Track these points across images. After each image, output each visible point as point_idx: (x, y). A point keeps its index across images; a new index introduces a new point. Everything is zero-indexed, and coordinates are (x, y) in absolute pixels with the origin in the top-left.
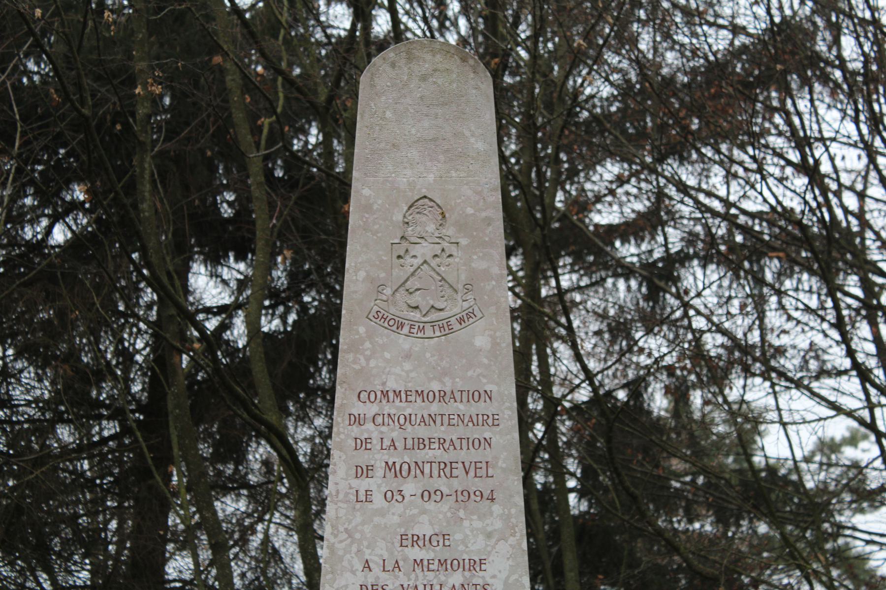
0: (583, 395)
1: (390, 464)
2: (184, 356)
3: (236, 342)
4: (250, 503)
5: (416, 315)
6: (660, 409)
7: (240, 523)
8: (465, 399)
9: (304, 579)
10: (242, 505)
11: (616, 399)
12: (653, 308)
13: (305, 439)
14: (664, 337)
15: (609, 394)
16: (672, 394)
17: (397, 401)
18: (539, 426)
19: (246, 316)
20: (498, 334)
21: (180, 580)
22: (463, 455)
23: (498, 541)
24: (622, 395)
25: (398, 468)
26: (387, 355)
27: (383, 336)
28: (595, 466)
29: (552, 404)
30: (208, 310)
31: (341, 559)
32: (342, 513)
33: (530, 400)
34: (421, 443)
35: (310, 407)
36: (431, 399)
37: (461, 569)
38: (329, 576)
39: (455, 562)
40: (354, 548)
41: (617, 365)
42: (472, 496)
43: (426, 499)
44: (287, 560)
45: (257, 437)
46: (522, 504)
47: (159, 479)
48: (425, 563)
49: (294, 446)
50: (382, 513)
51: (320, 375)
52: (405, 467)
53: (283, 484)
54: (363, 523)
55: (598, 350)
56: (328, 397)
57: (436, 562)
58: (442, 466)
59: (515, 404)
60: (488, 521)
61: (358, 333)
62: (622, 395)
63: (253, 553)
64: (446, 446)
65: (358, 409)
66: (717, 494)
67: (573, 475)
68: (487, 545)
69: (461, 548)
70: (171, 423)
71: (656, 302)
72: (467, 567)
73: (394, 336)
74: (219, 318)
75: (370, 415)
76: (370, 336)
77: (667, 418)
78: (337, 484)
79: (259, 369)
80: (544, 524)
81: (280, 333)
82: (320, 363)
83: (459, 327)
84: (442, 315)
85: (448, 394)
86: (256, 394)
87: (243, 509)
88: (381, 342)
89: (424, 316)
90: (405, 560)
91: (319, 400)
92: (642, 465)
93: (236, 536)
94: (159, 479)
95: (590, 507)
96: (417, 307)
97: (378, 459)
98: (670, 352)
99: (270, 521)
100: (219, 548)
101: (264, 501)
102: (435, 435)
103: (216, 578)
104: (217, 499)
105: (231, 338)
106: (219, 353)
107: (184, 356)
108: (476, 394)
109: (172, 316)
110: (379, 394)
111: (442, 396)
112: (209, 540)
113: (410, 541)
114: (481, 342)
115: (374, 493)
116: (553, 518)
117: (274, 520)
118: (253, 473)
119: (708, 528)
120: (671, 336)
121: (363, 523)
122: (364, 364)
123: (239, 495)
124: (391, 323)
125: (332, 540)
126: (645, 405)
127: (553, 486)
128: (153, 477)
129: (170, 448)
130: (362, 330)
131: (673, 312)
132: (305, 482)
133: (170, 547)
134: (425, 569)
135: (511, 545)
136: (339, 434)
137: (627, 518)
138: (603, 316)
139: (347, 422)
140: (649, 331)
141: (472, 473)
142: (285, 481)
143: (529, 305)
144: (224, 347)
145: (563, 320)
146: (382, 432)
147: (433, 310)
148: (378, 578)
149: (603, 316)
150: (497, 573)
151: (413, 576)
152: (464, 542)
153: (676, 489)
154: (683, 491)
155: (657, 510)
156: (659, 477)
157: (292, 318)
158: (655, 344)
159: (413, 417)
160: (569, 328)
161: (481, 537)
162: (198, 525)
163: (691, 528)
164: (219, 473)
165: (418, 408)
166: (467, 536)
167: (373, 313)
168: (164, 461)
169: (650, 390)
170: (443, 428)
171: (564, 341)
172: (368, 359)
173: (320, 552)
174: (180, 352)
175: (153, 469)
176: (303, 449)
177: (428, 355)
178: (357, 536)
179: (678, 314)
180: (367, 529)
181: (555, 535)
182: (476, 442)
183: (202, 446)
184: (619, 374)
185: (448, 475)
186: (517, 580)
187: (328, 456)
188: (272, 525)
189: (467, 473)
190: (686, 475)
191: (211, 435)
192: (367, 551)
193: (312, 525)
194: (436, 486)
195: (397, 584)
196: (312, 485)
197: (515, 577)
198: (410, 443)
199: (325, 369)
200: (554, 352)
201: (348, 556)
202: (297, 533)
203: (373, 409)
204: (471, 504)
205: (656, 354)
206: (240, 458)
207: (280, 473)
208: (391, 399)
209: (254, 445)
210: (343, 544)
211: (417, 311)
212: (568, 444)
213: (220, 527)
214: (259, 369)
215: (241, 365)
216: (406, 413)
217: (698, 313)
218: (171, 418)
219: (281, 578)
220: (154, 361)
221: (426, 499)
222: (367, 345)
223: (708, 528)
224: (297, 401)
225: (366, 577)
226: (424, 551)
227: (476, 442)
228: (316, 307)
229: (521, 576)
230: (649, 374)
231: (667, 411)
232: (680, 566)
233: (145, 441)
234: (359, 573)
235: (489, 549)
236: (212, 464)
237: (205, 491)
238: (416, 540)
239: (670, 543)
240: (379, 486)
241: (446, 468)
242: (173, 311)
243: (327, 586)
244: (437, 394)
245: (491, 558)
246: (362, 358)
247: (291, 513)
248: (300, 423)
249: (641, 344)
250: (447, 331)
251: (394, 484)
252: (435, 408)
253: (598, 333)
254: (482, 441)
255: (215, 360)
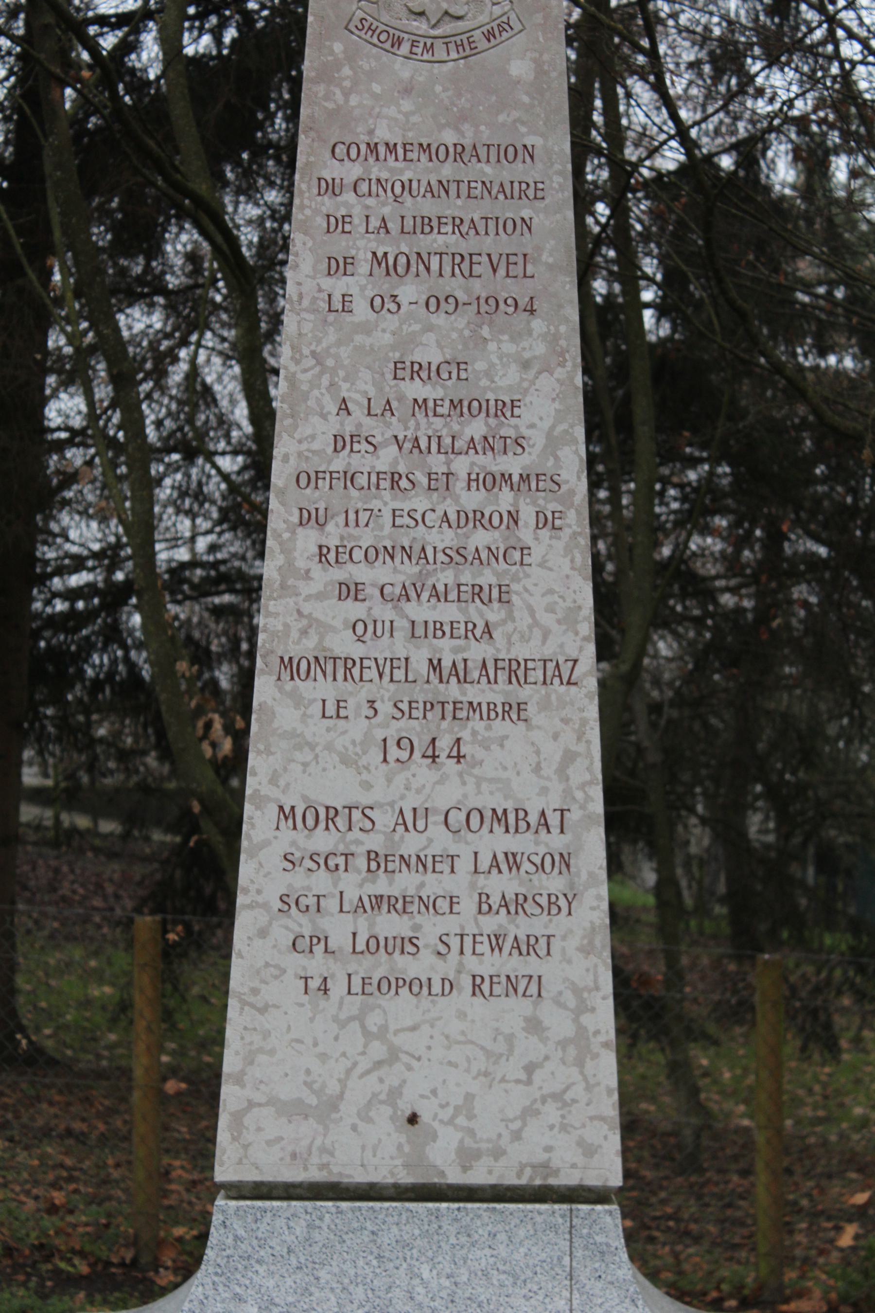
0: (671, 158)
1: (380, 255)
2: (69, 91)
3: (145, 70)
4: (167, 318)
5: (420, 26)
6: (783, 185)
7: (153, 346)
8: (493, 158)
9: (249, 429)
10: (157, 320)
11: (718, 168)
12: (780, 26)
13: (250, 222)
14: (796, 70)
15: (709, 159)
16: (804, 160)
17: (391, 159)
18: (601, 208)
19: (160, 31)
20: (546, 57)
21: (67, 429)
22: (488, 243)
23: (540, 373)
24: (726, 162)
25: (433, 151)
26: (376, 88)
27: (371, 58)
28: (684, 268)
29: (622, 171)
30: (102, 20)
31: (305, 397)
32: (307, 328)
33: (588, 169)
34: (427, 225)
35: (258, 175)
36: (442, 156)
37: (483, 414)
38: (288, 422)
39: (475, 404)
40: (325, 381)
41: (721, 115)
42: (502, 305)
43: (433, 308)
44: (224, 403)
45: (178, 217)
46: (577, 318)
47: (32, 276)
48: (431, 404)
49: (235, 232)
50: (366, 329)
51: (273, 124)
52: (402, 260)
53: (218, 290)
54: (339, 343)
55: (694, 91)
56: (284, 158)
57: (447, 403)
58: (458, 259)
59: (569, 167)
60: (525, 344)
61: (332, 52)
62: (726, 162)
63: (174, 392)
64: (464, 229)
65: (332, 170)
66: (865, 314)
67: (651, 280)
68: (522, 380)
69: (484, 382)
70: (50, 195)
71: (784, 17)
72: (492, 411)
73: (386, 57)
74: (120, 34)
75: (349, 180)
76: (351, 57)
77: (792, 198)
78: (299, 284)
79: (181, 113)
80: (606, 354)
81: (212, 58)
82: (273, 106)
83: (486, 45)
84: (461, 25)
85: (469, 149)
86: (178, 152)
87: (158, 326)
88: (366, 67)
89: (434, 27)
90: (401, 399)
91: (271, 163)
92: (754, 268)
93: (149, 366)
94: (32, 276)
95: (674, 330)
96: (422, 14)
97: (362, 247)
98: (803, 94)
99: (199, 345)
100: (123, 380)
101: (189, 314)
102: (448, 212)
103: (119, 428)
104: (121, 311)
105: (138, 65)
106: (121, 86)
107: (69, 91)
108: (511, 150)
109: (47, 26)
110: (363, 147)
111: (459, 152)
112: (109, 370)
113: (408, 371)
114: (520, 68)
115: (354, 299)
116: (617, 347)
117: (203, 343)
118: (173, 273)
119: (848, 363)
120: (806, 69)
121: (339, 343)
122: (341, 102)
123: (152, 305)
124: (383, 37)
125: (293, 368)
126: (763, 177)
127: (620, 300)
128: (24, 274)
129: (49, 231)
130: (338, 47)
131: (811, 30)
132: (250, 284)
133: (51, 380)
134: (430, 414)
135: (558, 380)
136: (302, 207)
137: (727, 345)
138: (704, 38)
139: (315, 191)
140: (772, 61)
141: (502, 272)
142: (221, 284)
143: (593, 16)
144: (127, 79)
145: (645, 43)
146: (368, 207)
147: (447, 19)
148: (359, 425)
149: (704, 38)
150: (536, 420)
151: (412, 423)
152: (488, 374)
153: (804, 305)
154: (814, 307)
155: (773, 336)
156: (779, 285)
157: (230, 34)
158: (781, 84)
159: (415, 185)
160: (652, 53)
161: (514, 367)
162: (92, 349)
163: (823, 364)
164: (123, 272)
165: (422, 170)
166: (492, 365)
167: (356, 21)
168: (41, 251)
169: (770, 154)
170: (459, 202)
171: (644, 78)
172: (346, 94)
173: (273, 392)
174: (64, 84)
175: (24, 261)
176: (248, 236)
177: (438, 88)
178: (330, 363)
179: (818, 34)
180: (344, 352)
181: (621, 371)
182: (510, 224)
183: (95, 230)
184: (724, 129)
185: (467, 274)
186: (566, 432)
187: (285, 248)
188: (201, 351)
189: (495, 271)
190: (820, 283)
191: (110, 213)
192: (345, 386)
193: (261, 351)
194: (448, 290)
195: (389, 434)
196: (260, 293)
197: (564, 426)
198: (409, 223)
199: (280, 115)
200: (629, 95)
201: (316, 392)
202: (239, 362)
203: (354, 171)
204: (500, 318)
205: (783, 95)
206: (155, 250)
207: (213, 272)
208: (382, 156)
209: (174, 229)
210: (309, 375)
211: (423, 19)
212: (646, 237)
213: (126, 351)
214: (181, 113)
215: (152, 104)
216: (405, 179)
217: (851, 35)
218: (49, 184)
219: (215, 429)
220: (22, 96)
221: (433, 308)
222: (347, 71)
223: (848, 363)
224: (237, 163)
225: (342, 424)
226: (428, 387)
227: (510, 224)
228: (265, 19)
229: (572, 426)
230: (771, 129)
231: (794, 187)
232: (804, 420)
233: (11, 218)
234: (332, 418)
235: (525, 385)
236: (111, 257)
237: (103, 297)
238: (416, 371)
239: (795, 384)
240: (363, 288)
241: (464, 263)
242: (49, 19)
243: (285, 436)
244: (451, 150)
245: (528, 399)
246: (338, 92)
247: (231, 334)
248: (242, 198)
249: (759, 80)
250: (468, 52)
251: (386, 286)
252: (447, 171)
253: (693, 66)
254: (519, 222)
255: (115, 97)
